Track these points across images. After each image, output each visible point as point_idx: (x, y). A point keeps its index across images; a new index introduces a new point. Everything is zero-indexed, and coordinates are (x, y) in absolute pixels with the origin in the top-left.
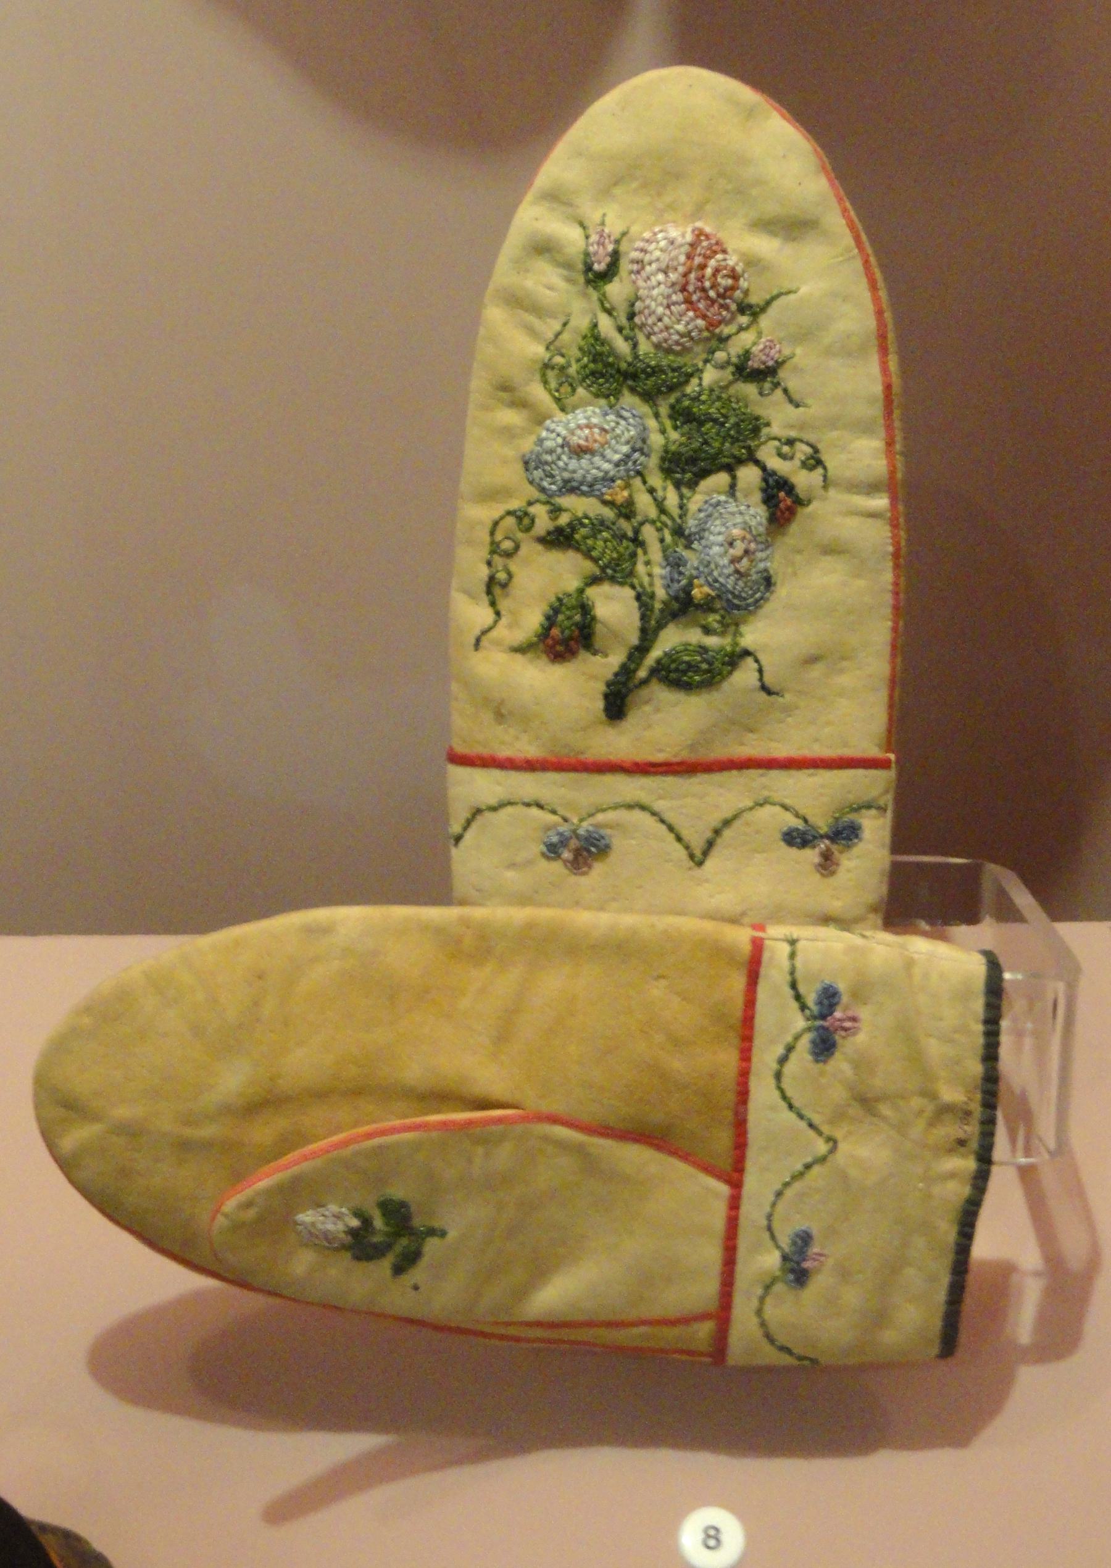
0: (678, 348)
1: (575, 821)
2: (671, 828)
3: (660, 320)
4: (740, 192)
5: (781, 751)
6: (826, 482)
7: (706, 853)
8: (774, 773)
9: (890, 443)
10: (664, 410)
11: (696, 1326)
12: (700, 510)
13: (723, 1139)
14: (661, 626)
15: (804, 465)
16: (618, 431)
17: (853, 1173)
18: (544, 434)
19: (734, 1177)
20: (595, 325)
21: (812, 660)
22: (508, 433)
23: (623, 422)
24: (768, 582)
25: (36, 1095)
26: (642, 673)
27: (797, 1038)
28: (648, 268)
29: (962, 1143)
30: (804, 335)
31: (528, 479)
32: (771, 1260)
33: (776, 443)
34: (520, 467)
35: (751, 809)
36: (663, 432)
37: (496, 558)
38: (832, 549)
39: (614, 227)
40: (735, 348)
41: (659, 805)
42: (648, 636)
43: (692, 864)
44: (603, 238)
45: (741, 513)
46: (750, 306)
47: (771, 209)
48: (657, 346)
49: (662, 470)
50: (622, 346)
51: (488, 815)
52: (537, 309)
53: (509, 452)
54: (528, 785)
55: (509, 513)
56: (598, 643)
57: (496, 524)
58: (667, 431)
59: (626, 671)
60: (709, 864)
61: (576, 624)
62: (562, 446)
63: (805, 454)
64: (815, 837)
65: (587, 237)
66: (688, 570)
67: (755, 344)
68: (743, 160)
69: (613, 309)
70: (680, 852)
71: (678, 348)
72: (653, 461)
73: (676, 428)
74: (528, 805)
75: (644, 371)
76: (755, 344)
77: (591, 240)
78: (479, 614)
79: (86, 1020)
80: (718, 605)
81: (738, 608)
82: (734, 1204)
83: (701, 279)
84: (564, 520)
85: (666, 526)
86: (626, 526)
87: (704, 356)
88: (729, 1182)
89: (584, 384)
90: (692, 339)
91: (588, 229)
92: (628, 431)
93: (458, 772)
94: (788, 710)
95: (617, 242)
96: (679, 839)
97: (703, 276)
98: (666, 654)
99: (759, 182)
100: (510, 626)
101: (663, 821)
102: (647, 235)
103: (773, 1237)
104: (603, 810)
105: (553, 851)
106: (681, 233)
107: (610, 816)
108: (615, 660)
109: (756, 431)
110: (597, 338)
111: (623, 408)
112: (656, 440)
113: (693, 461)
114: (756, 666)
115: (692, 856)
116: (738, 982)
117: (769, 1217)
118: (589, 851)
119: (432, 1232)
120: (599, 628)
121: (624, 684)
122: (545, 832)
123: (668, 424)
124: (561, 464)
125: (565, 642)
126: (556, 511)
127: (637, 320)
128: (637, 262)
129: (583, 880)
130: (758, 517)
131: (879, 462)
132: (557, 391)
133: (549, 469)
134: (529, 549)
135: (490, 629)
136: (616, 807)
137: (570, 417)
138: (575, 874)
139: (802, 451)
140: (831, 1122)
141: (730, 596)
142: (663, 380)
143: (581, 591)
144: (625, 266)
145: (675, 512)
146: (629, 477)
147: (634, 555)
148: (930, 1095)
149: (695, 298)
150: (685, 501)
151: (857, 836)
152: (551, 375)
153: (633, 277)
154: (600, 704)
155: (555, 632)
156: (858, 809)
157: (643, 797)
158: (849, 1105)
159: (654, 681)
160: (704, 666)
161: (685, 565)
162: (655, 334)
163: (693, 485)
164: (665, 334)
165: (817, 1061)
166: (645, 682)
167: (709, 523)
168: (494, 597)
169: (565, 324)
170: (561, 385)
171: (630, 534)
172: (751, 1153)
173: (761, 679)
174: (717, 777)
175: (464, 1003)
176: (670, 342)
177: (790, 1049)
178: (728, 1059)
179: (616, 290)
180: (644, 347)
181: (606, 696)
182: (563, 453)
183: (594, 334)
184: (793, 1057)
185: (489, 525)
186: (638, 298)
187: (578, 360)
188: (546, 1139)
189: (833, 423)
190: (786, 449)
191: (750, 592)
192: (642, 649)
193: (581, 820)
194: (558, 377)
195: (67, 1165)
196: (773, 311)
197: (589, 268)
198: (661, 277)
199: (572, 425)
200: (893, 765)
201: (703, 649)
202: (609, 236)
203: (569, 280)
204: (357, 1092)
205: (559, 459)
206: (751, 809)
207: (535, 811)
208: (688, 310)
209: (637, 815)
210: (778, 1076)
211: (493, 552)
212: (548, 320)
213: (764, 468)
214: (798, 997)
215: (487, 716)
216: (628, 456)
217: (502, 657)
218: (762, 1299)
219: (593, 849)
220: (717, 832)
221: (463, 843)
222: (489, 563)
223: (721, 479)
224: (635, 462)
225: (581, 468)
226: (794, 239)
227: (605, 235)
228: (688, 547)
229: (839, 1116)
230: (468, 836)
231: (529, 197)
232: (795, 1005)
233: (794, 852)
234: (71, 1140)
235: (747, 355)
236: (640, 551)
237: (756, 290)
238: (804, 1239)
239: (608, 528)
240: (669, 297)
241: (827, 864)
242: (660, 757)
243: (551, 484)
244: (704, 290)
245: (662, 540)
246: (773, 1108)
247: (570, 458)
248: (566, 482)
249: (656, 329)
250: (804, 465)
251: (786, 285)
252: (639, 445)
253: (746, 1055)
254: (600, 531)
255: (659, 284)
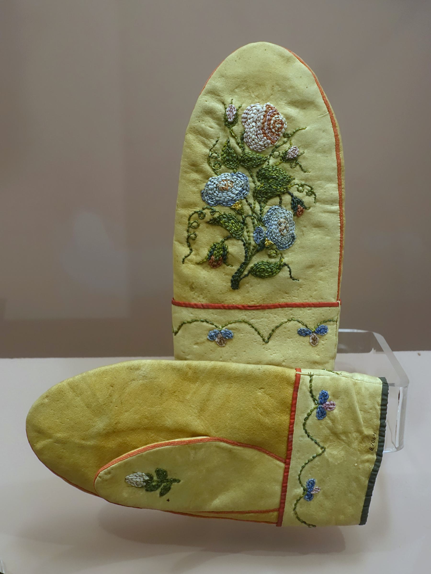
0: (260, 151)
1: (220, 327)
2: (256, 330)
3: (253, 140)
4: (284, 91)
5: (297, 300)
6: (316, 200)
7: (269, 339)
8: (295, 309)
9: (339, 185)
10: (255, 175)
11: (271, 513)
12: (268, 212)
13: (283, 447)
14: (253, 255)
15: (307, 194)
16: (237, 182)
17: (330, 460)
18: (209, 183)
19: (287, 460)
20: (229, 142)
21: (311, 266)
22: (195, 182)
23: (239, 179)
24: (293, 238)
25: (27, 427)
26: (246, 273)
27: (312, 411)
28: (249, 120)
29: (372, 449)
30: (307, 146)
31: (203, 200)
32: (300, 491)
33: (297, 186)
34: (199, 195)
35: (286, 322)
36: (254, 182)
37: (190, 229)
38: (319, 226)
39: (236, 105)
40: (282, 150)
41: (252, 321)
42: (248, 259)
43: (264, 343)
44: (231, 109)
45: (284, 213)
46: (288, 134)
47: (297, 97)
48: (253, 150)
49: (254, 196)
50: (239, 150)
51: (188, 325)
52: (206, 135)
53: (195, 189)
54: (203, 314)
55: (195, 212)
56: (229, 261)
57: (190, 216)
58: (256, 182)
59: (240, 272)
60: (270, 343)
61: (221, 255)
62: (216, 188)
63: (308, 190)
64: (310, 333)
65: (226, 108)
66: (263, 234)
67: (289, 149)
68: (286, 79)
69: (236, 136)
70: (261, 339)
71: (260, 151)
72: (250, 194)
73: (259, 181)
74: (202, 321)
75: (247, 159)
76: (289, 149)
77: (227, 110)
78: (184, 250)
79: (46, 400)
80: (275, 247)
81: (283, 248)
82: (286, 471)
83: (269, 125)
84: (216, 215)
85: (255, 218)
86: (240, 218)
87: (271, 153)
88: (285, 463)
89: (224, 164)
90: (265, 147)
91: (226, 105)
92: (241, 182)
93: (175, 308)
94: (300, 286)
95: (237, 110)
96: (259, 334)
97: (270, 124)
98: (255, 265)
99: (291, 87)
100: (196, 255)
101: (253, 327)
102: (249, 108)
103: (300, 482)
104: (231, 323)
105: (212, 338)
106: (261, 107)
107: (233, 325)
108: (235, 268)
109: (289, 182)
110: (229, 147)
111: (239, 173)
112: (252, 185)
113: (266, 193)
114: (288, 269)
115: (264, 340)
116: (290, 390)
117: (299, 475)
118: (225, 338)
119: (175, 480)
120: (229, 256)
121: (239, 276)
122: (209, 332)
123: (256, 179)
124: (215, 194)
125: (216, 261)
126: (213, 212)
127: (244, 140)
128: (245, 118)
129: (223, 349)
130: (290, 215)
131: (335, 192)
132: (214, 166)
133: (211, 196)
134: (203, 226)
135: (189, 255)
136: (235, 322)
137: (219, 176)
138: (221, 347)
139: (307, 189)
140: (323, 442)
141: (279, 244)
142: (254, 163)
143: (223, 242)
144: (240, 120)
145: (259, 212)
146: (241, 199)
147: (242, 229)
148: (360, 432)
149: (267, 132)
150: (263, 208)
151: (326, 332)
152: (212, 160)
153: (243, 124)
154: (230, 284)
155: (213, 257)
156: (325, 322)
157: (245, 318)
158: (330, 435)
159: (250, 275)
160: (269, 270)
161: (262, 233)
162: (251, 145)
163: (265, 202)
164: (255, 146)
165: (319, 419)
166: (246, 276)
167: (272, 217)
168: (190, 243)
169: (217, 141)
170: (215, 164)
171: (242, 221)
172: (294, 453)
173: (290, 274)
174: (273, 311)
175: (188, 397)
176: (257, 148)
177: (309, 415)
178: (286, 418)
179: (237, 129)
180: (247, 150)
181: (232, 281)
182: (216, 190)
183: (228, 145)
184: (310, 418)
185: (188, 217)
186: (245, 132)
187: (222, 155)
188: (218, 447)
189: (319, 178)
190: (301, 188)
191: (287, 242)
192: (245, 264)
193: (223, 327)
194: (215, 161)
195: (39, 453)
196: (296, 136)
197: (226, 120)
198: (254, 124)
199: (220, 180)
200: (340, 305)
201: (269, 264)
202: (234, 108)
203: (218, 124)
204: (147, 429)
205: (215, 192)
206: (286, 322)
207: (205, 324)
208: (264, 136)
209: (243, 325)
210: (304, 425)
211: (189, 227)
212: (211, 140)
213: (292, 196)
214: (312, 396)
215: (187, 288)
216: (241, 192)
217: (192, 266)
218: (296, 505)
219: (227, 338)
220: (273, 331)
221: (178, 334)
222: (188, 231)
223: (277, 200)
224: (243, 194)
225: (224, 196)
226: (304, 109)
227: (232, 108)
228: (264, 226)
229: (326, 439)
230: (180, 332)
231: (203, 92)
232: (311, 399)
233: (302, 338)
234: (39, 445)
235: (286, 153)
236: (245, 227)
237: (288, 128)
238: (312, 483)
239: (233, 219)
240: (257, 132)
241: (314, 342)
242: (252, 303)
243: (211, 202)
244: (270, 129)
245: (253, 223)
246: (302, 436)
247: (219, 192)
248: (217, 201)
249: (252, 144)
250: (307, 194)
251: (302, 126)
252: (245, 187)
253: (292, 418)
254: (231, 220)
255: (253, 126)
